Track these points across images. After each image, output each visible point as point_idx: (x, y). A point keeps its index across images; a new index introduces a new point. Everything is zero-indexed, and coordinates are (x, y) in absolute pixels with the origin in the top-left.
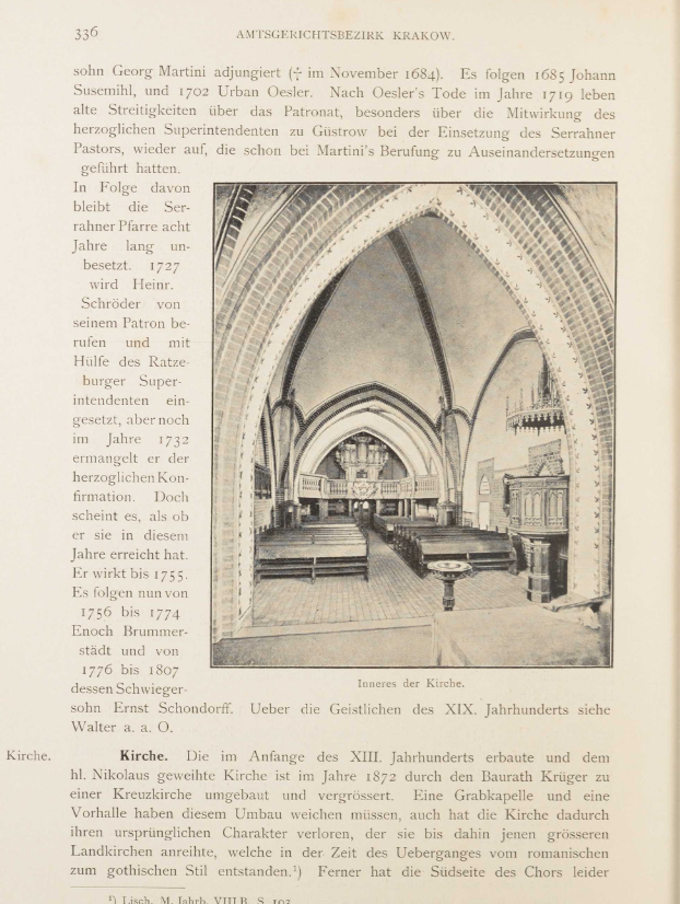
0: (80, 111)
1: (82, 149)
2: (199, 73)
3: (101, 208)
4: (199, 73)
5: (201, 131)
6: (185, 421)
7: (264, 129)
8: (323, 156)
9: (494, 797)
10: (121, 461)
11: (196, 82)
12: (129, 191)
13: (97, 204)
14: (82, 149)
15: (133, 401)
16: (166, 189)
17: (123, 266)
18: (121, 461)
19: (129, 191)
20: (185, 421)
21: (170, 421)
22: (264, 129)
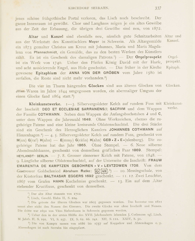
0: (139, 24)
1: (38, 145)
2: (142, 104)
3: (147, 18)
4: (142, 104)
5: (120, 42)
6: (127, 18)
7: (41, 145)
8: (117, 48)
9: (41, 151)
10: (92, 58)
11: (141, 107)
12: (30, 146)
13: (146, 17)
14: (38, 145)
15: (127, 156)
16: (125, 63)
17: (104, 68)
18: (92, 58)
19: (30, 146)
20: (127, 18)
21: (123, 18)
22: (41, 145)
